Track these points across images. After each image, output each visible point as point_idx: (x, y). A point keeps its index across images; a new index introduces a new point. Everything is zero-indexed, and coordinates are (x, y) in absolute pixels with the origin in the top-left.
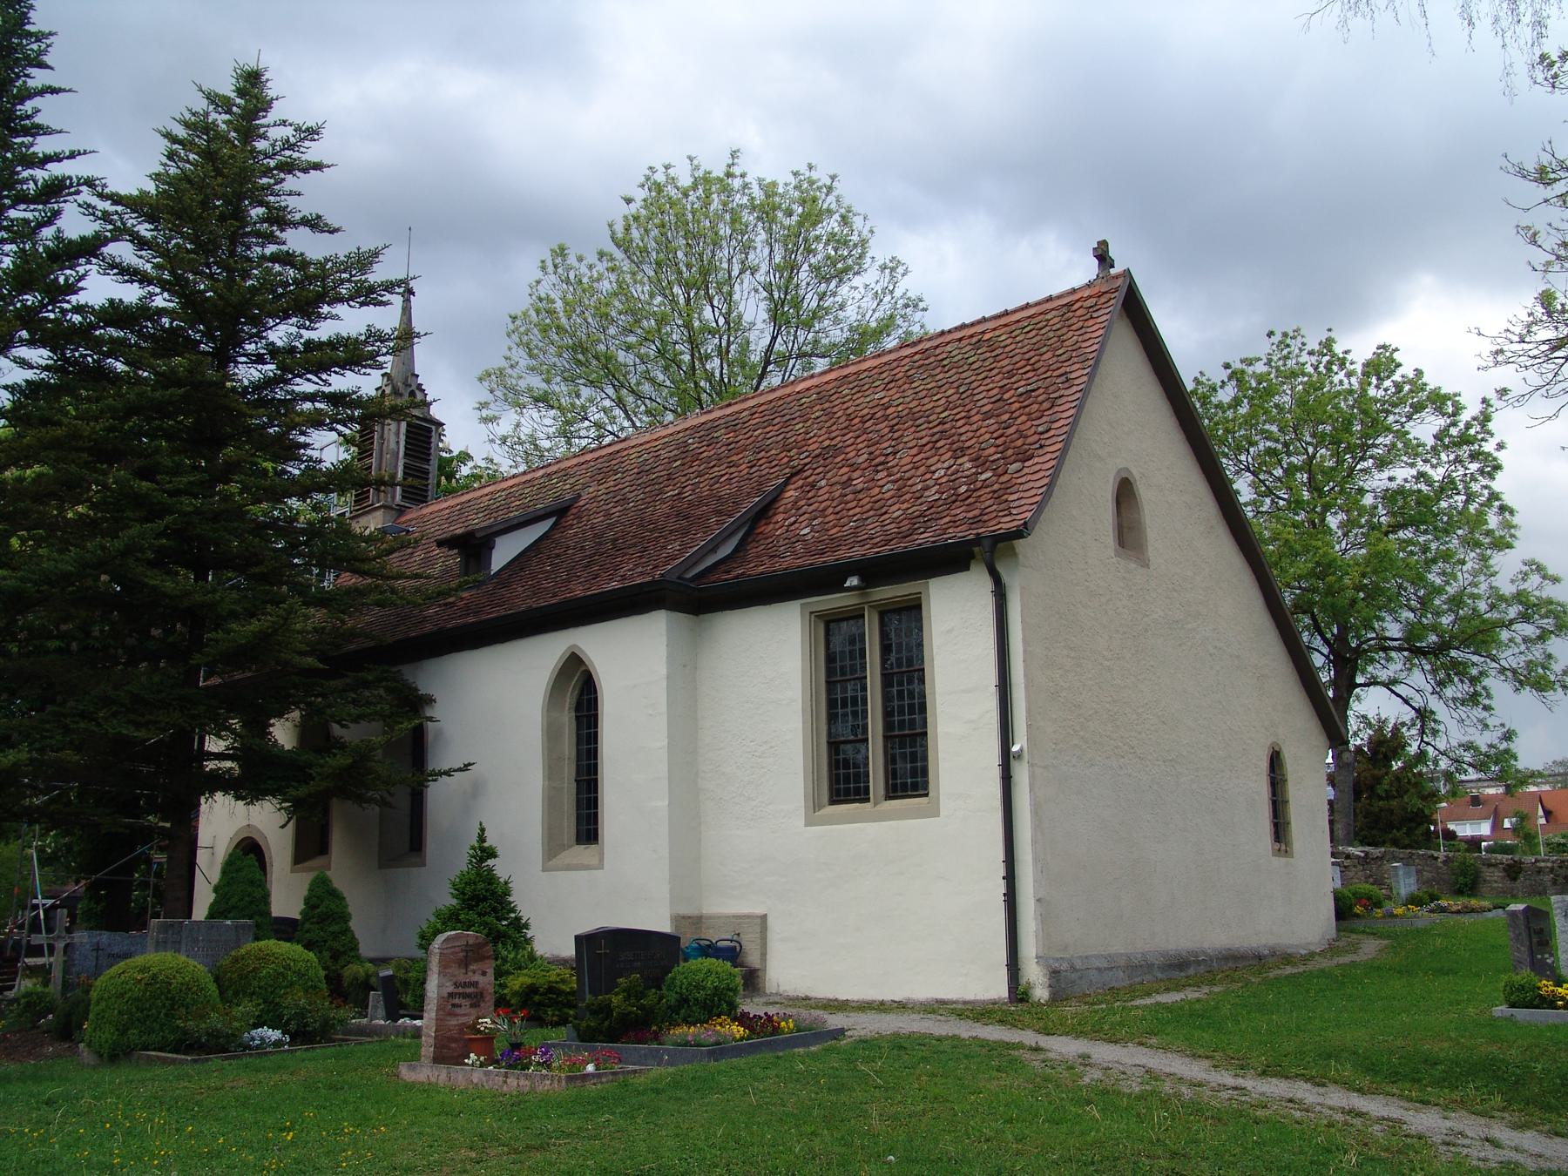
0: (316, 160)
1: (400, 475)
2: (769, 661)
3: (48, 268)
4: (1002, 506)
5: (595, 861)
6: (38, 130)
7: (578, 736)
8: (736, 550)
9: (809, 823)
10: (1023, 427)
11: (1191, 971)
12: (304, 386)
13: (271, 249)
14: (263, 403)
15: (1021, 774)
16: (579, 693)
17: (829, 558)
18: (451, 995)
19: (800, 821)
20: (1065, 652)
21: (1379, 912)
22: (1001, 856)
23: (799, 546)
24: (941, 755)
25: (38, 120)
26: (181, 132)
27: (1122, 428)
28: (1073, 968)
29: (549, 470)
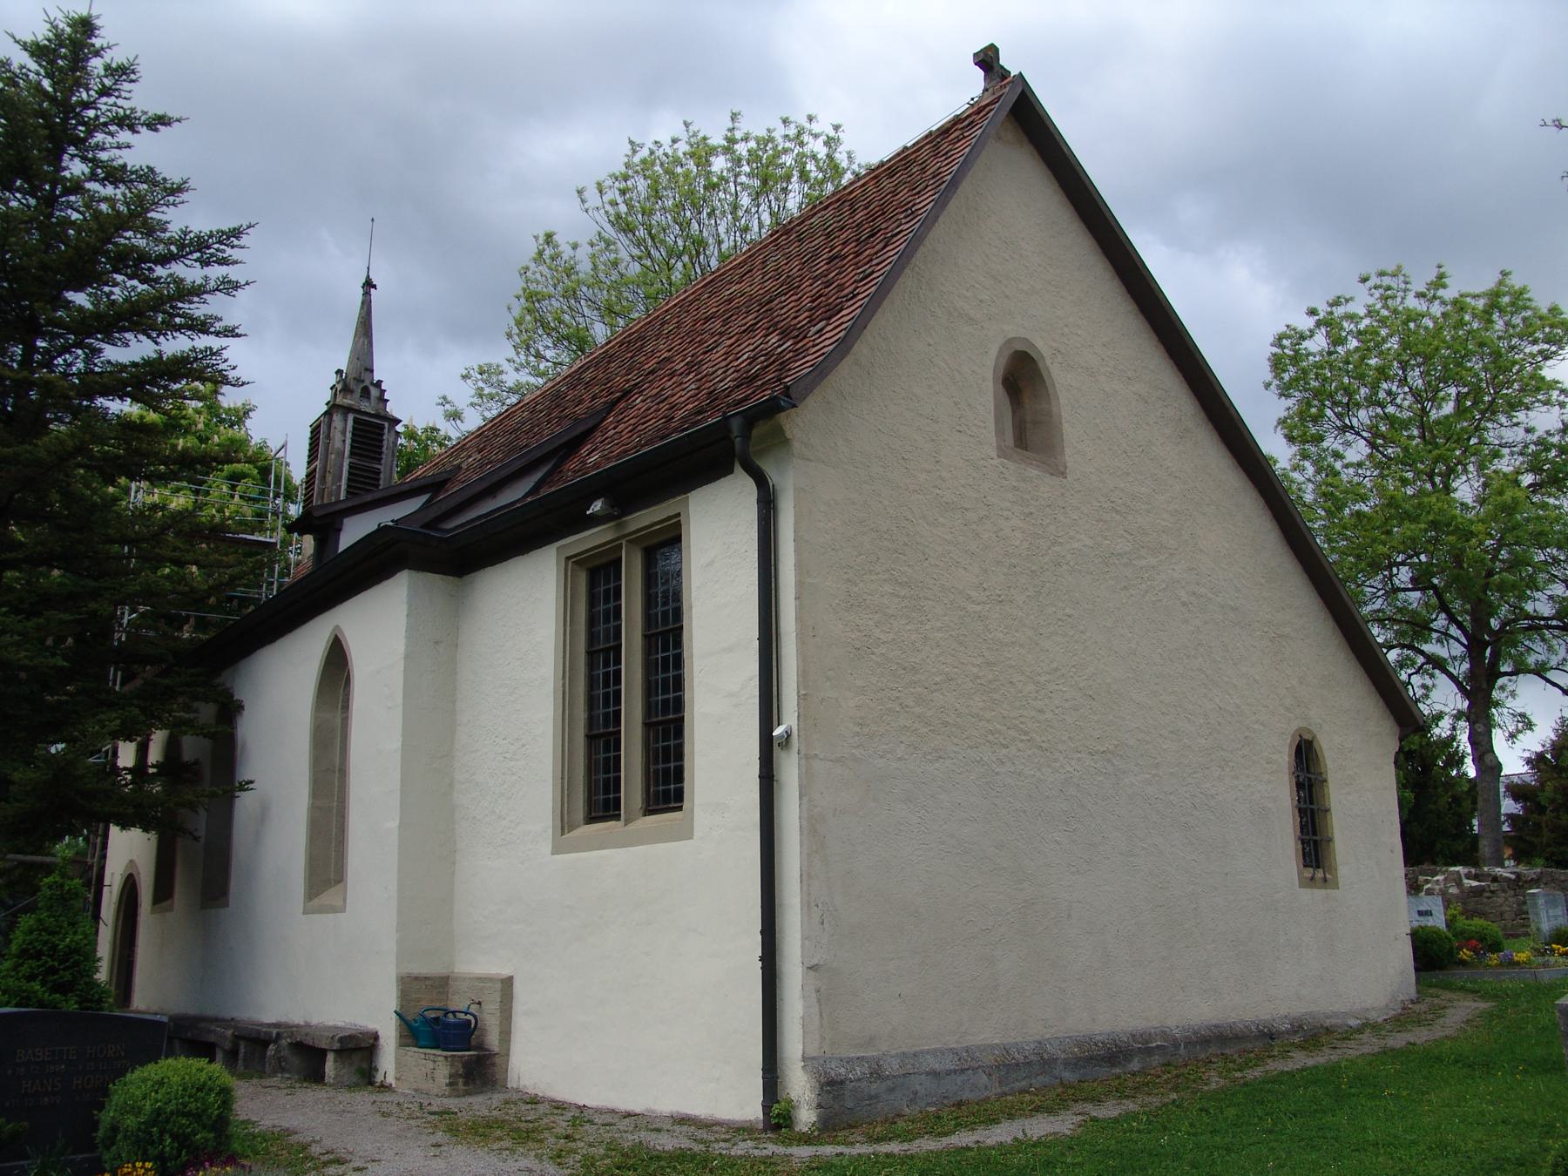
11: (1135, 1065)
19: (547, 847)
20: (888, 588)
21: (1494, 959)
24: (696, 749)
27: (1000, 271)
28: (877, 1074)
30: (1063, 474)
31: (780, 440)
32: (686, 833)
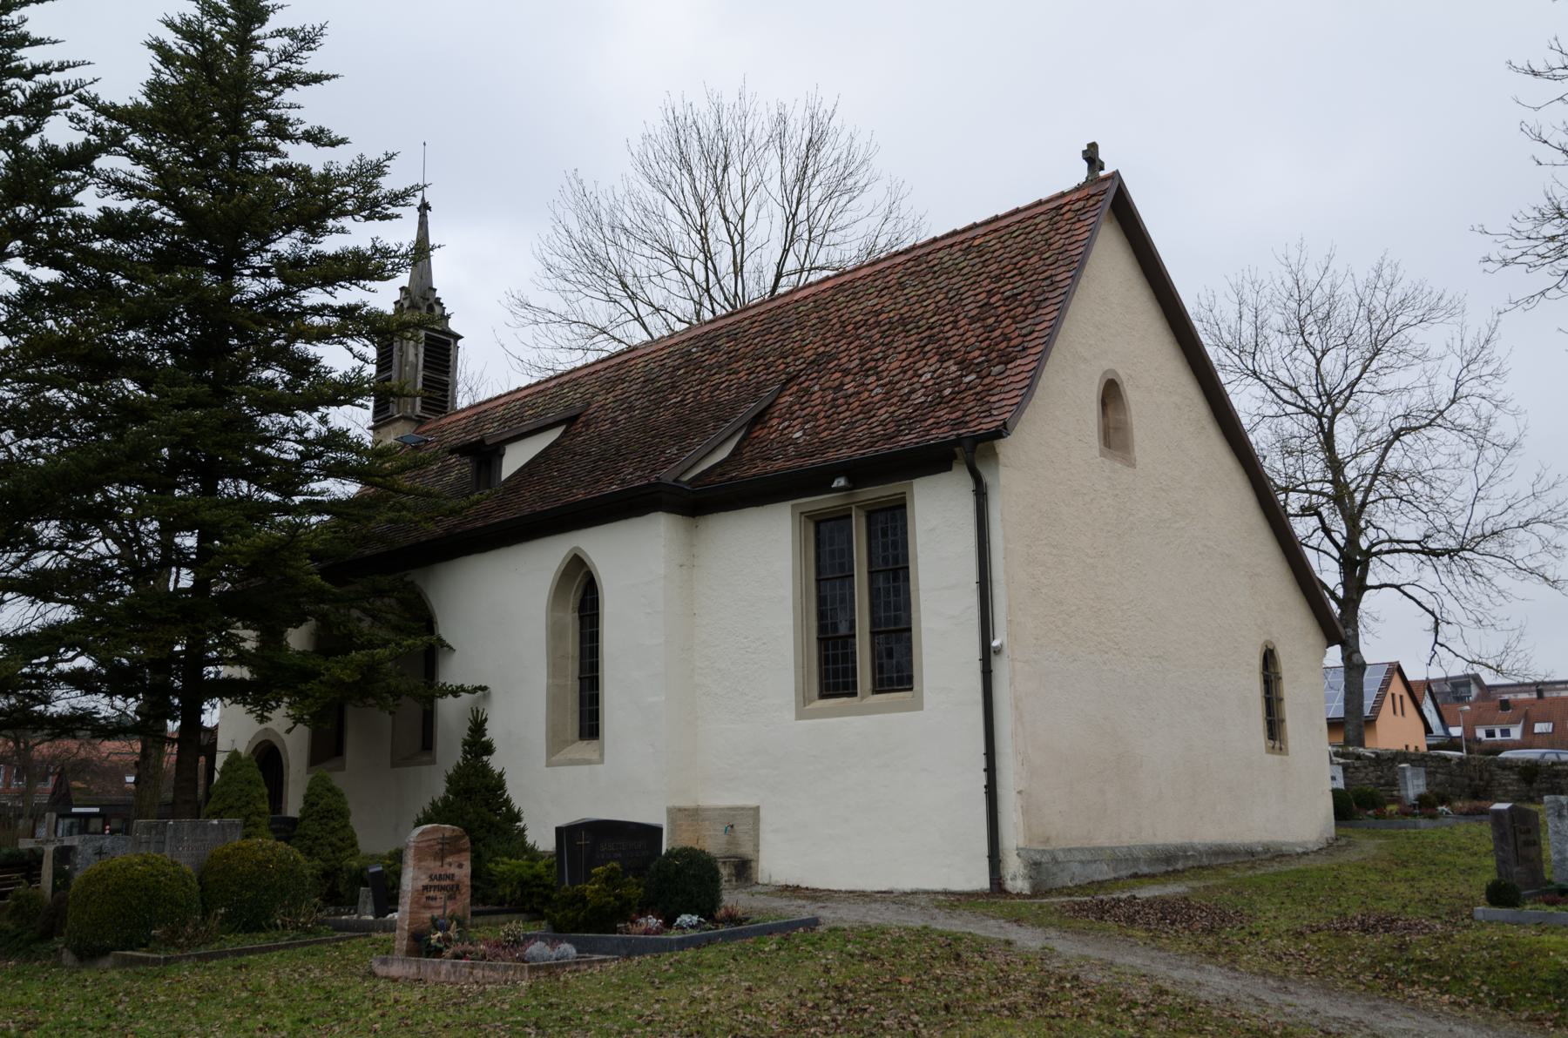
0: (316, 71)
1: (420, 386)
2: (762, 557)
3: (44, 176)
4: (985, 407)
5: (595, 757)
6: (24, 40)
7: (582, 635)
8: (733, 454)
9: (800, 716)
10: (1007, 331)
12: (314, 297)
13: (271, 163)
14: (273, 314)
15: (1001, 667)
16: (581, 593)
17: (817, 460)
18: (425, 888)
22: (982, 749)
23: (791, 449)
25: (24, 29)
26: (171, 39)
27: (1102, 320)
28: (1055, 861)
29: (562, 380)
30: (1134, 466)
31: (993, 455)
32: (918, 706)
